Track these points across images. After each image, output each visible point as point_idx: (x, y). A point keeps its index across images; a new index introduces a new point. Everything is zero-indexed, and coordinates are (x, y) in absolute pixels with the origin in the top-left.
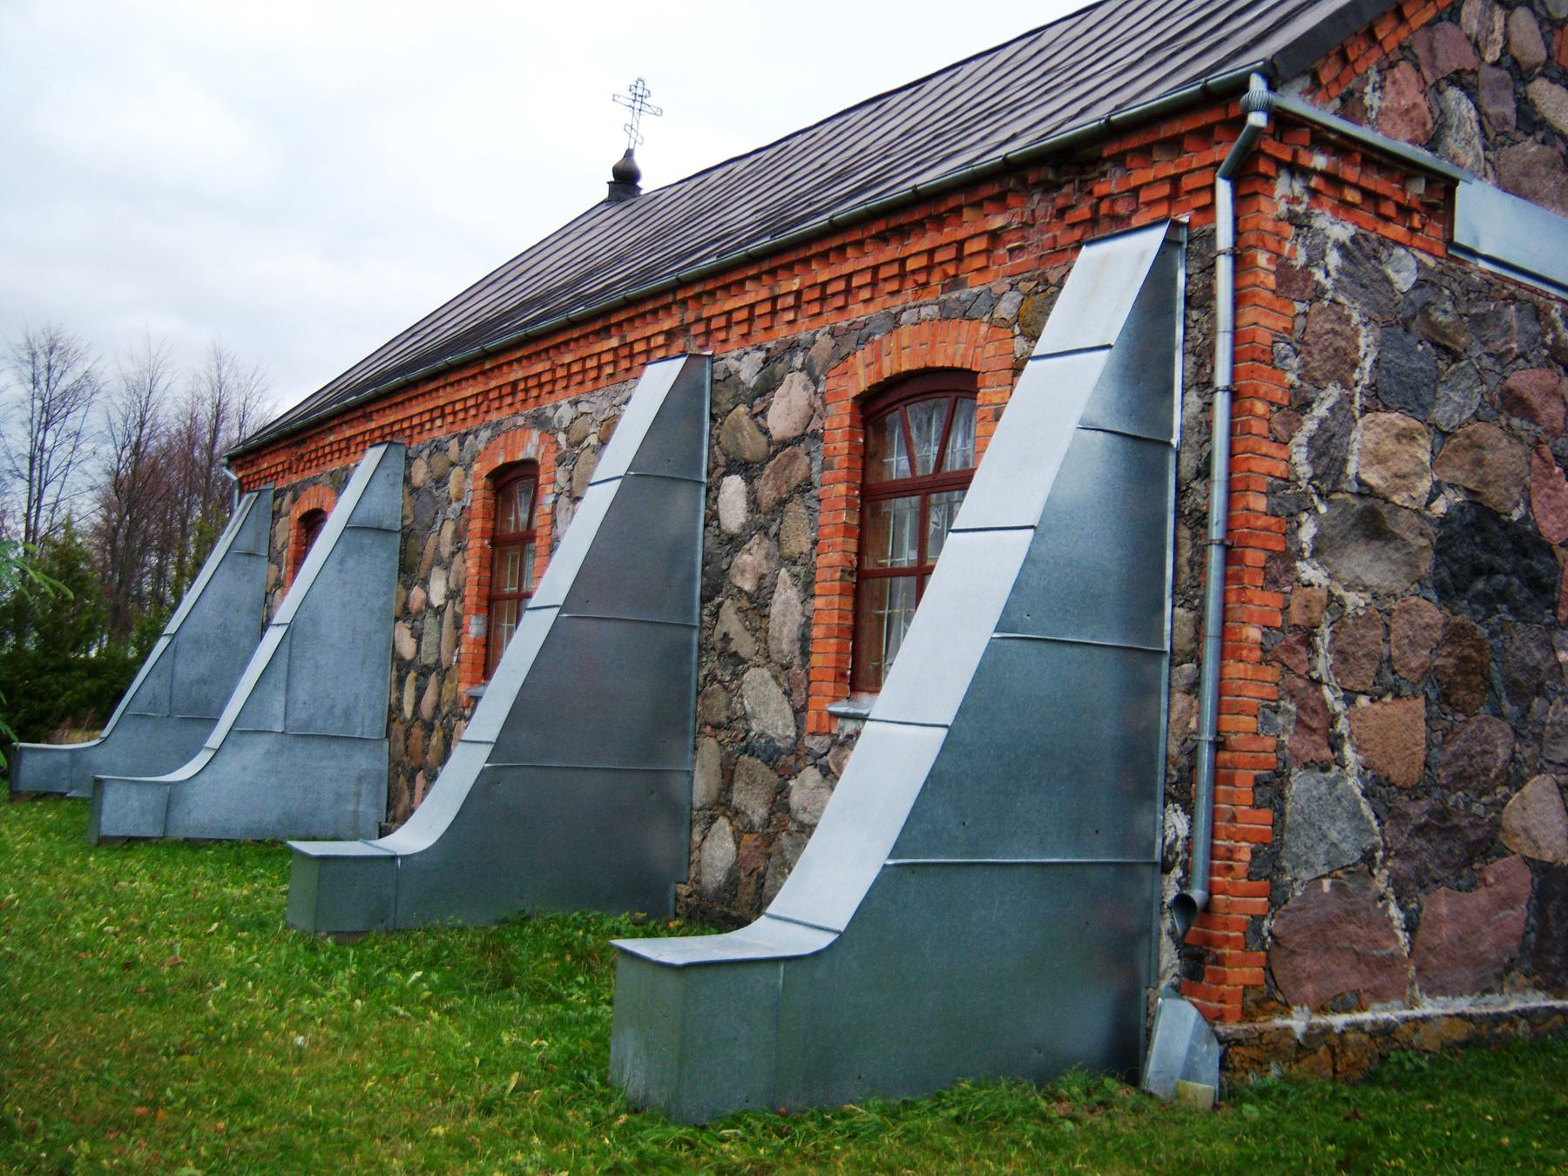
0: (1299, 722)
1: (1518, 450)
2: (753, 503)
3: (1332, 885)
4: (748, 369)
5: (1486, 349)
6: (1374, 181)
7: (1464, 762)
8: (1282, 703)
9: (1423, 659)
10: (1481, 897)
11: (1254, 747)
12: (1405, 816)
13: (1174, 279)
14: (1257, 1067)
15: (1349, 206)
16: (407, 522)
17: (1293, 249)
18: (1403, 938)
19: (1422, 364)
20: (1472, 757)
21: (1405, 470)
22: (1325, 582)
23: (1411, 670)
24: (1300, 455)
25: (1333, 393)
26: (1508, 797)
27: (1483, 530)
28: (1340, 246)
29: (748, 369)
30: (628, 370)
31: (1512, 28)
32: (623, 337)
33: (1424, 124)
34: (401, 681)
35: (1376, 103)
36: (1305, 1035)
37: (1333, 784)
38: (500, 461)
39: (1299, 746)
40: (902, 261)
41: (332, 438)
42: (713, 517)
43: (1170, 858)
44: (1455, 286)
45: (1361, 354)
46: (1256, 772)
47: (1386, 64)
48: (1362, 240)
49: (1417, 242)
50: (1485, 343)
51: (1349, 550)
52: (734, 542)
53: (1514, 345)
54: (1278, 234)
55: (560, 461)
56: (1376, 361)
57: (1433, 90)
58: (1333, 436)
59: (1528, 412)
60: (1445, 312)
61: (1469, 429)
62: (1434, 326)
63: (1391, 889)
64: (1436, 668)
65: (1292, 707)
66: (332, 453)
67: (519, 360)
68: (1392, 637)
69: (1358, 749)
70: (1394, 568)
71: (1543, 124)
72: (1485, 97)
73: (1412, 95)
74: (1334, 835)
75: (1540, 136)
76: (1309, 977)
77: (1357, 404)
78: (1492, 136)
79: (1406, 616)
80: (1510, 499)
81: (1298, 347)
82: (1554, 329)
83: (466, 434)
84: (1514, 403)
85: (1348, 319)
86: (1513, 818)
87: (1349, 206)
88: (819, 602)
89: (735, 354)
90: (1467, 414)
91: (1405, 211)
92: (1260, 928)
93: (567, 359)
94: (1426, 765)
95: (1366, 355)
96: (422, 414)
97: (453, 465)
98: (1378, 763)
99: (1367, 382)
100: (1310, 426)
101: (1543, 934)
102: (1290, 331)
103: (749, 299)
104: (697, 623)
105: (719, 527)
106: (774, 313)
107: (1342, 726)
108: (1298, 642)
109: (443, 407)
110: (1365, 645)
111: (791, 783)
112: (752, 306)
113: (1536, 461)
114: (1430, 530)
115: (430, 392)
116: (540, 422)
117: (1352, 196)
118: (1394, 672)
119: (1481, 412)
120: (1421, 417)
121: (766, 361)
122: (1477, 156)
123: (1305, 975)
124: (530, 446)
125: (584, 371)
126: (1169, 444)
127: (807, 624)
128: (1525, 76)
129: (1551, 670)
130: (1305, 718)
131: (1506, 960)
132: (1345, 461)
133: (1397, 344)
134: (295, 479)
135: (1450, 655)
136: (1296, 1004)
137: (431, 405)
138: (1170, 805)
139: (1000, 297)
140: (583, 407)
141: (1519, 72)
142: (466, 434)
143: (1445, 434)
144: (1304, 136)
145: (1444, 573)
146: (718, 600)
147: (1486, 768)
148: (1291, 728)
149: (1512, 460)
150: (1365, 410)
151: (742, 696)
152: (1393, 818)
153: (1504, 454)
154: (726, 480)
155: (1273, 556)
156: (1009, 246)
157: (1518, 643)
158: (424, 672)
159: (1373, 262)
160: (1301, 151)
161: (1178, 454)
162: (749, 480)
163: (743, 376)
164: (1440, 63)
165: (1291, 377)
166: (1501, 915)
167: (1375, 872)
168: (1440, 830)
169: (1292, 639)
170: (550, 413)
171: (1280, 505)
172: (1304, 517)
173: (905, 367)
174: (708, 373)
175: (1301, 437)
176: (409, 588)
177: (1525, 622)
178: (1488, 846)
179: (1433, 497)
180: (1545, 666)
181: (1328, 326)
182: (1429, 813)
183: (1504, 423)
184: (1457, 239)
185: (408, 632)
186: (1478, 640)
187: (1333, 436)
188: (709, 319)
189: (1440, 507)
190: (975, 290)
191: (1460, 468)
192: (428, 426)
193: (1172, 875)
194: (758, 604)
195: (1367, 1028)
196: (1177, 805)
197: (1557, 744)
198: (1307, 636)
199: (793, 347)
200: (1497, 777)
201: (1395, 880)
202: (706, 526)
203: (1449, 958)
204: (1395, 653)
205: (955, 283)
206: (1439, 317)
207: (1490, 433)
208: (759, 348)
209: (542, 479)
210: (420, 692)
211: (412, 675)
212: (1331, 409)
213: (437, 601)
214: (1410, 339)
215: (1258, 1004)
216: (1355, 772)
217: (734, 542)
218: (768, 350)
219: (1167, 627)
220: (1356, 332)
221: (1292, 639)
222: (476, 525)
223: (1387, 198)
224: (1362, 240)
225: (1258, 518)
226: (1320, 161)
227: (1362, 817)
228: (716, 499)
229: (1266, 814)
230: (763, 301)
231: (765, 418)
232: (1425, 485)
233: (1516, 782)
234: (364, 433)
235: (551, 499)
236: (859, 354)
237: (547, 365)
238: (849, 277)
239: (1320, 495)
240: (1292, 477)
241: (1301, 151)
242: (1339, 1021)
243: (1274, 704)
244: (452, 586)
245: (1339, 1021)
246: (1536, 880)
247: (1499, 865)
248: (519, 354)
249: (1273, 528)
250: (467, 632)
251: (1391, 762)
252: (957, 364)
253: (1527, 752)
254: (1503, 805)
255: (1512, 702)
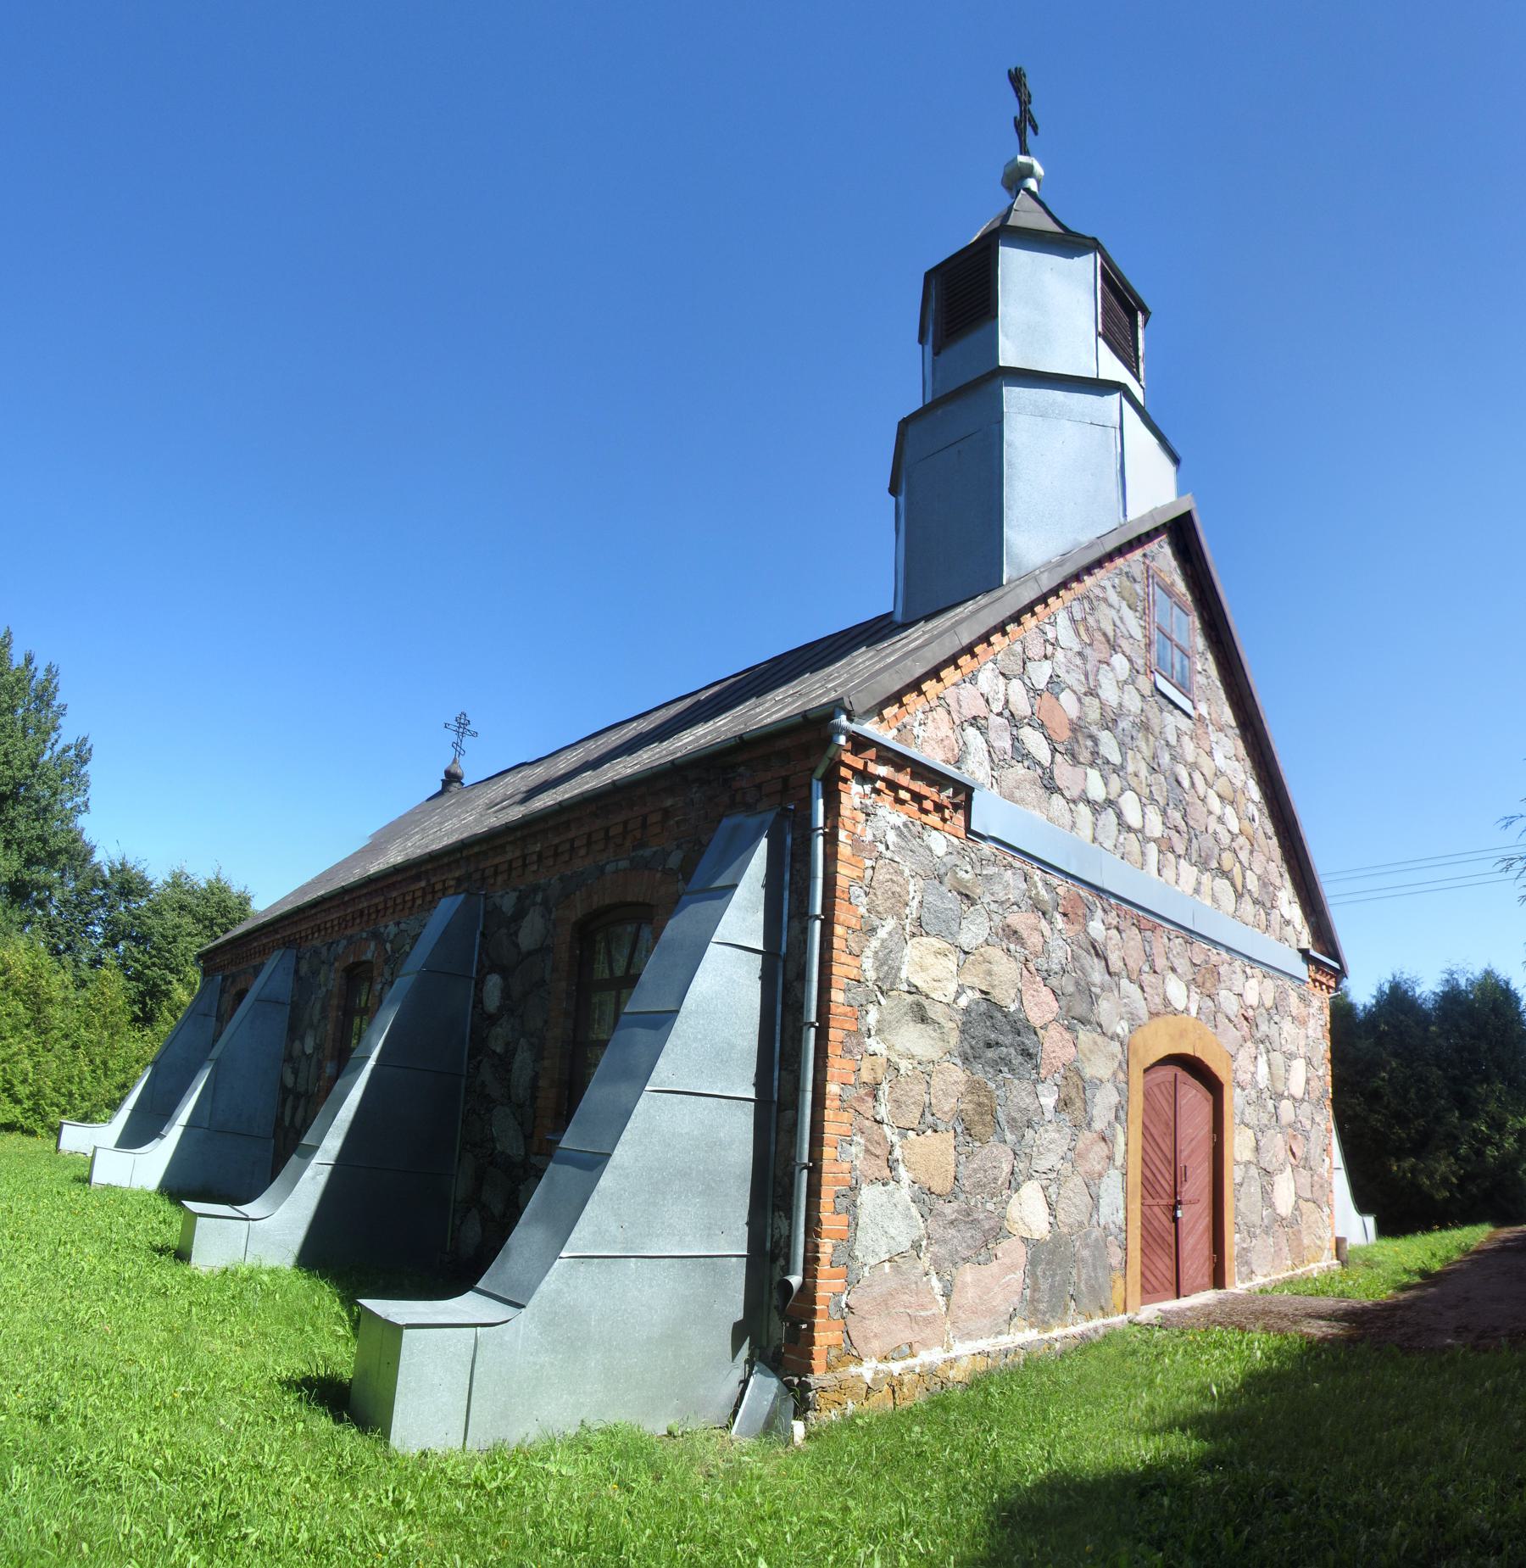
0: (867, 1151)
1: (1014, 965)
2: (506, 993)
3: (891, 1267)
4: (508, 903)
5: (993, 898)
6: (919, 787)
7: (980, 1175)
8: (855, 1138)
9: (952, 1105)
10: (994, 1266)
11: (834, 1170)
12: (942, 1214)
13: (785, 840)
14: (838, 1406)
15: (901, 802)
16: (295, 998)
17: (864, 830)
18: (942, 1301)
19: (951, 906)
20: (985, 1171)
21: (941, 977)
22: (885, 1053)
23: (946, 1113)
24: (868, 963)
25: (890, 923)
26: (1010, 1197)
27: (992, 1017)
28: (895, 828)
29: (508, 903)
30: (430, 902)
31: (1010, 692)
32: (428, 881)
33: (953, 750)
34: (284, 1101)
35: (921, 734)
36: (873, 1380)
37: (891, 1195)
38: (351, 960)
39: (867, 1168)
40: (607, 830)
41: (255, 944)
42: (479, 1001)
43: (777, 1251)
44: (973, 855)
45: (911, 897)
46: (838, 1188)
47: (928, 709)
48: (910, 825)
49: (947, 827)
50: (992, 894)
51: (902, 1031)
52: (492, 1019)
53: (1010, 896)
54: (853, 819)
55: (387, 961)
56: (921, 903)
57: (960, 728)
58: (891, 951)
59: (1020, 940)
60: (967, 872)
61: (982, 950)
62: (960, 881)
63: (932, 1267)
64: (962, 1111)
65: (862, 1141)
66: (255, 953)
67: (365, 895)
68: (932, 1090)
69: (909, 1169)
70: (932, 1042)
71: (1028, 755)
72: (992, 735)
73: (945, 730)
74: (892, 1232)
75: (1026, 763)
76: (875, 1336)
77: (907, 931)
78: (996, 761)
79: (941, 1076)
80: (1009, 997)
81: (867, 889)
82: (1036, 887)
83: (332, 943)
84: (1013, 934)
85: (902, 873)
86: (1013, 1211)
87: (901, 802)
88: (546, 1063)
89: (500, 893)
90: (981, 940)
91: (939, 808)
92: (840, 1302)
93: (394, 894)
94: (956, 1178)
95: (913, 898)
96: (307, 929)
97: (323, 962)
98: (923, 1179)
99: (914, 916)
100: (875, 943)
101: (1035, 1289)
102: (861, 878)
103: (509, 856)
104: (465, 1073)
105: (482, 1008)
106: (525, 865)
107: (897, 1153)
108: (866, 1094)
109: (319, 925)
110: (913, 1096)
111: (521, 1187)
112: (510, 862)
113: (1025, 972)
114: (957, 1017)
115: (312, 915)
116: (376, 936)
117: (904, 795)
118: (933, 1115)
119: (990, 939)
120: (951, 942)
121: (519, 898)
122: (987, 773)
123: (872, 1334)
124: (370, 953)
125: (405, 902)
126: (779, 955)
127: (536, 1077)
128: (1018, 724)
129: (1036, 1110)
130: (871, 1148)
131: (1011, 1309)
132: (899, 969)
133: (935, 892)
134: (234, 969)
135: (970, 1101)
136: (866, 1356)
137: (312, 924)
138: (776, 1214)
139: (669, 854)
140: (403, 926)
141: (1014, 721)
142: (332, 943)
143: (966, 953)
144: (872, 753)
145: (967, 1047)
146: (479, 1058)
147: (995, 1179)
148: (861, 1155)
149: (1009, 971)
150: (913, 935)
151: (491, 1125)
152: (934, 1216)
153: (1005, 970)
154: (489, 977)
155: (849, 1033)
156: (676, 819)
157: (1015, 1093)
158: (298, 1096)
159: (918, 840)
160: (869, 763)
161: (785, 962)
162: (505, 979)
163: (504, 909)
164: (963, 711)
165: (862, 910)
166: (1007, 1278)
167: (921, 1255)
168: (966, 1222)
169: (862, 1092)
170: (382, 930)
171: (853, 998)
172: (870, 1007)
173: (607, 902)
174: (482, 906)
175: (868, 952)
176: (293, 1041)
177: (1019, 1079)
178: (998, 1232)
179: (958, 994)
180: (1032, 1108)
181: (888, 877)
182: (958, 1211)
183: (1005, 947)
184: (973, 827)
185: (290, 1070)
186: (989, 1092)
187: (891, 951)
188: (484, 870)
189: (963, 1002)
190: (654, 849)
191: (977, 976)
192: (310, 937)
193: (778, 1263)
194: (504, 1063)
195: (918, 1370)
196: (781, 1213)
197: (1040, 1159)
198: (874, 1091)
199: (535, 889)
200: (1003, 1184)
201: (935, 1261)
202: (474, 1007)
203: (973, 1313)
204: (934, 1101)
205: (641, 845)
206: (961, 874)
207: (996, 953)
208: (514, 890)
209: (375, 973)
210: (295, 1109)
211: (291, 1097)
212: (890, 933)
213: (309, 1051)
214: (944, 889)
215: (838, 1358)
216: (907, 1185)
217: (492, 1019)
218: (520, 891)
219: (776, 1083)
220: (908, 882)
221: (862, 1092)
222: (334, 1002)
223: (926, 798)
224: (910, 825)
225: (838, 1007)
226: (883, 771)
227: (911, 1218)
228: (481, 990)
229: (844, 1218)
230: (518, 858)
231: (517, 937)
232: (952, 988)
233: (1013, 1184)
234: (273, 941)
235: (379, 987)
236: (578, 893)
237: (382, 898)
238: (572, 841)
239: (882, 993)
240: (862, 980)
241: (869, 763)
242: (896, 1367)
243: (848, 1138)
244: (318, 1041)
245: (896, 1367)
246: (1029, 1252)
247: (1005, 1244)
248: (365, 891)
249: (849, 1014)
250: (324, 1072)
251: (932, 1177)
252: (641, 900)
253: (1021, 1166)
254: (1007, 1203)
255: (1012, 1132)
